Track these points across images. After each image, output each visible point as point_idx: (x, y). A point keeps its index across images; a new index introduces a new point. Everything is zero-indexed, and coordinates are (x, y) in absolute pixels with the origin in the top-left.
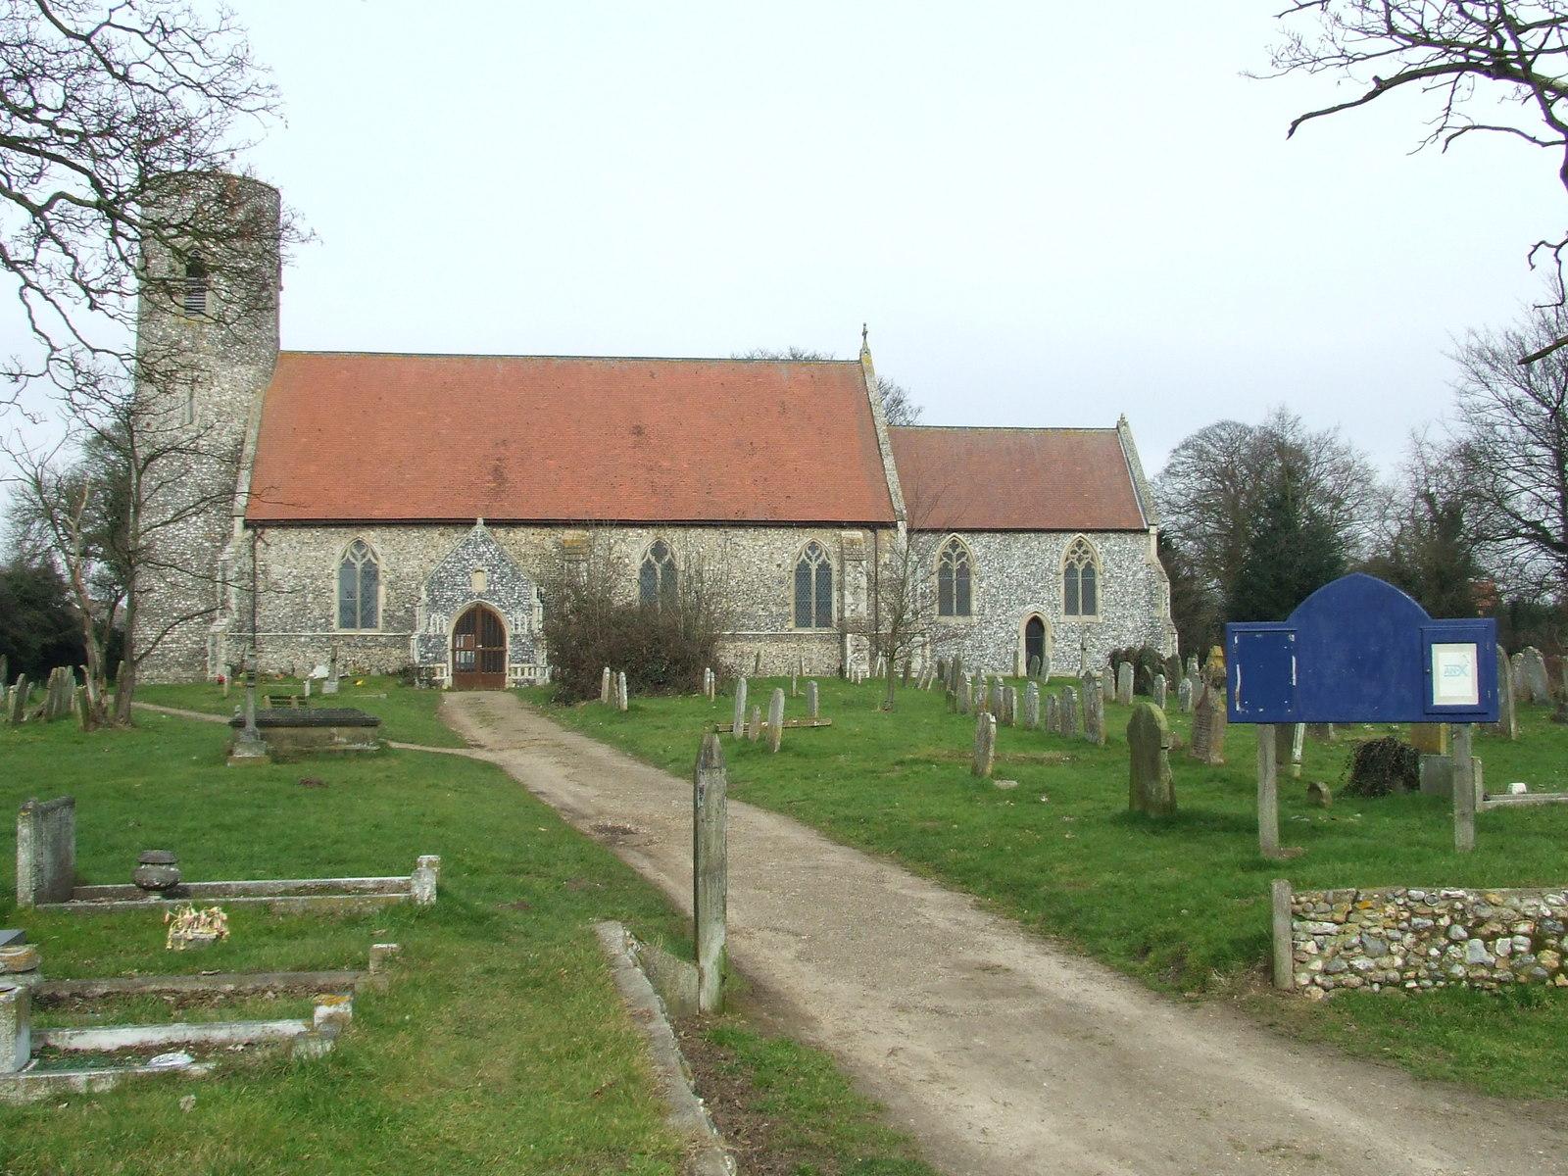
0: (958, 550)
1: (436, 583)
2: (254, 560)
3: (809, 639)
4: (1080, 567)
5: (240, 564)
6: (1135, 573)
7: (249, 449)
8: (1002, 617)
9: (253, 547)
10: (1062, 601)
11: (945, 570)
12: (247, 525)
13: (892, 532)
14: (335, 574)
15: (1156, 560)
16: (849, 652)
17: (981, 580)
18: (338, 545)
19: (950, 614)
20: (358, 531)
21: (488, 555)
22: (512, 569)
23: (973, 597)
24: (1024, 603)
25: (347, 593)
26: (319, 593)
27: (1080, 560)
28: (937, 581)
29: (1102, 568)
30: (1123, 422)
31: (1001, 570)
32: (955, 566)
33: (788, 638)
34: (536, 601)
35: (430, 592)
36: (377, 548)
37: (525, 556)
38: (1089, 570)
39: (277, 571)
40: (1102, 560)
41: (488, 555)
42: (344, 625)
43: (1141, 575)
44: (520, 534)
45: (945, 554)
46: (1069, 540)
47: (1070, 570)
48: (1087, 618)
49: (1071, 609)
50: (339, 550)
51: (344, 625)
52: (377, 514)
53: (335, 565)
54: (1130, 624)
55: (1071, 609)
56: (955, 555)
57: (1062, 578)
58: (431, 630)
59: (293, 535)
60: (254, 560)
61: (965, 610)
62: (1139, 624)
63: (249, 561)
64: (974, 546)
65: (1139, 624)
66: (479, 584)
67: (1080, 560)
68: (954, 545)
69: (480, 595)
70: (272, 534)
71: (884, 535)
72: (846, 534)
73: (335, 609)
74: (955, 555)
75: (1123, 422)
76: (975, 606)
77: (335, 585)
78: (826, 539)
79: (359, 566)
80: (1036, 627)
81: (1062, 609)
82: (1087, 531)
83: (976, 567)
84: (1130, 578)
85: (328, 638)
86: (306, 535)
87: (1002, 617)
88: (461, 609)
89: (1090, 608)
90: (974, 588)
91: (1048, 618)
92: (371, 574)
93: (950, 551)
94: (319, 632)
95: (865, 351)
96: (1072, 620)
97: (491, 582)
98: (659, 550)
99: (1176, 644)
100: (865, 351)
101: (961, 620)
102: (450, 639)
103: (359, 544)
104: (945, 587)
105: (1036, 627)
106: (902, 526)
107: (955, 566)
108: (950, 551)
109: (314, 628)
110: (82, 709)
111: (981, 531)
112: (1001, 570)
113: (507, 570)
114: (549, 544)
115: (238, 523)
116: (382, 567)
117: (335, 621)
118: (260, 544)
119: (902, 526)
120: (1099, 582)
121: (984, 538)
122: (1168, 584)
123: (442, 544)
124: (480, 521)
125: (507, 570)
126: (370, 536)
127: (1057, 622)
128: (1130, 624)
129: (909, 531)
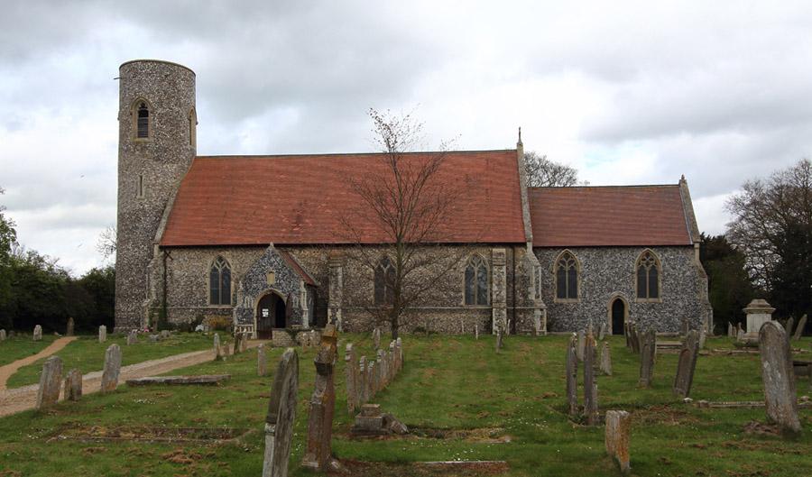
0: (570, 259)
1: (247, 279)
2: (166, 268)
3: (473, 311)
4: (648, 269)
5: (157, 269)
6: (684, 272)
7: (168, 209)
8: (597, 299)
9: (164, 261)
10: (636, 289)
11: (561, 272)
12: (161, 248)
13: (523, 249)
14: (208, 275)
15: (699, 264)
16: (494, 319)
17: (584, 277)
18: (209, 259)
19: (565, 297)
20: (220, 251)
21: (276, 263)
22: (289, 271)
23: (579, 287)
24: (610, 290)
25: (214, 283)
26: (199, 285)
27: (647, 264)
28: (556, 279)
29: (662, 270)
30: (683, 181)
31: (597, 271)
32: (567, 268)
33: (461, 311)
34: (303, 290)
35: (245, 285)
36: (229, 260)
37: (310, 264)
38: (654, 271)
39: (177, 273)
40: (662, 263)
41: (276, 263)
42: (212, 303)
43: (688, 273)
44: (307, 252)
45: (561, 262)
46: (640, 253)
47: (641, 271)
48: (651, 300)
49: (641, 294)
50: (209, 263)
51: (212, 303)
52: (230, 242)
53: (208, 270)
54: (681, 304)
55: (641, 294)
56: (567, 262)
57: (635, 276)
58: (245, 305)
59: (185, 254)
60: (166, 268)
61: (573, 295)
62: (687, 303)
63: (162, 269)
64: (580, 258)
65: (687, 303)
66: (271, 280)
67: (647, 264)
68: (567, 256)
69: (271, 286)
70: (174, 253)
71: (519, 250)
72: (495, 250)
73: (208, 294)
74: (567, 262)
75: (683, 181)
76: (579, 293)
77: (208, 281)
78: (483, 254)
79: (220, 270)
80: (618, 306)
81: (635, 294)
82: (652, 247)
83: (580, 269)
84: (681, 275)
85: (204, 310)
86: (192, 254)
87: (597, 299)
88: (261, 294)
89: (654, 294)
90: (579, 282)
91: (626, 299)
92: (227, 273)
93: (564, 259)
94: (199, 306)
95: (520, 144)
96: (641, 300)
97: (277, 279)
98: (567, 256)
99: (712, 316)
100: (520, 144)
101: (571, 300)
102: (255, 310)
103: (221, 259)
104: (561, 283)
105: (618, 306)
106: (530, 245)
107: (567, 268)
108: (564, 259)
109: (196, 304)
110: (177, 354)
111: (583, 248)
112: (597, 271)
113: (286, 271)
114: (323, 257)
115: (156, 247)
116: (233, 271)
117: (208, 300)
118: (168, 259)
119: (530, 245)
120: (660, 277)
121: (586, 253)
122: (706, 279)
123: (250, 257)
124: (272, 244)
125: (286, 271)
126: (227, 255)
127: (632, 301)
128: (681, 304)
129: (535, 249)
